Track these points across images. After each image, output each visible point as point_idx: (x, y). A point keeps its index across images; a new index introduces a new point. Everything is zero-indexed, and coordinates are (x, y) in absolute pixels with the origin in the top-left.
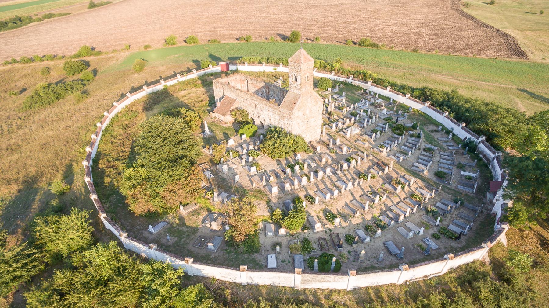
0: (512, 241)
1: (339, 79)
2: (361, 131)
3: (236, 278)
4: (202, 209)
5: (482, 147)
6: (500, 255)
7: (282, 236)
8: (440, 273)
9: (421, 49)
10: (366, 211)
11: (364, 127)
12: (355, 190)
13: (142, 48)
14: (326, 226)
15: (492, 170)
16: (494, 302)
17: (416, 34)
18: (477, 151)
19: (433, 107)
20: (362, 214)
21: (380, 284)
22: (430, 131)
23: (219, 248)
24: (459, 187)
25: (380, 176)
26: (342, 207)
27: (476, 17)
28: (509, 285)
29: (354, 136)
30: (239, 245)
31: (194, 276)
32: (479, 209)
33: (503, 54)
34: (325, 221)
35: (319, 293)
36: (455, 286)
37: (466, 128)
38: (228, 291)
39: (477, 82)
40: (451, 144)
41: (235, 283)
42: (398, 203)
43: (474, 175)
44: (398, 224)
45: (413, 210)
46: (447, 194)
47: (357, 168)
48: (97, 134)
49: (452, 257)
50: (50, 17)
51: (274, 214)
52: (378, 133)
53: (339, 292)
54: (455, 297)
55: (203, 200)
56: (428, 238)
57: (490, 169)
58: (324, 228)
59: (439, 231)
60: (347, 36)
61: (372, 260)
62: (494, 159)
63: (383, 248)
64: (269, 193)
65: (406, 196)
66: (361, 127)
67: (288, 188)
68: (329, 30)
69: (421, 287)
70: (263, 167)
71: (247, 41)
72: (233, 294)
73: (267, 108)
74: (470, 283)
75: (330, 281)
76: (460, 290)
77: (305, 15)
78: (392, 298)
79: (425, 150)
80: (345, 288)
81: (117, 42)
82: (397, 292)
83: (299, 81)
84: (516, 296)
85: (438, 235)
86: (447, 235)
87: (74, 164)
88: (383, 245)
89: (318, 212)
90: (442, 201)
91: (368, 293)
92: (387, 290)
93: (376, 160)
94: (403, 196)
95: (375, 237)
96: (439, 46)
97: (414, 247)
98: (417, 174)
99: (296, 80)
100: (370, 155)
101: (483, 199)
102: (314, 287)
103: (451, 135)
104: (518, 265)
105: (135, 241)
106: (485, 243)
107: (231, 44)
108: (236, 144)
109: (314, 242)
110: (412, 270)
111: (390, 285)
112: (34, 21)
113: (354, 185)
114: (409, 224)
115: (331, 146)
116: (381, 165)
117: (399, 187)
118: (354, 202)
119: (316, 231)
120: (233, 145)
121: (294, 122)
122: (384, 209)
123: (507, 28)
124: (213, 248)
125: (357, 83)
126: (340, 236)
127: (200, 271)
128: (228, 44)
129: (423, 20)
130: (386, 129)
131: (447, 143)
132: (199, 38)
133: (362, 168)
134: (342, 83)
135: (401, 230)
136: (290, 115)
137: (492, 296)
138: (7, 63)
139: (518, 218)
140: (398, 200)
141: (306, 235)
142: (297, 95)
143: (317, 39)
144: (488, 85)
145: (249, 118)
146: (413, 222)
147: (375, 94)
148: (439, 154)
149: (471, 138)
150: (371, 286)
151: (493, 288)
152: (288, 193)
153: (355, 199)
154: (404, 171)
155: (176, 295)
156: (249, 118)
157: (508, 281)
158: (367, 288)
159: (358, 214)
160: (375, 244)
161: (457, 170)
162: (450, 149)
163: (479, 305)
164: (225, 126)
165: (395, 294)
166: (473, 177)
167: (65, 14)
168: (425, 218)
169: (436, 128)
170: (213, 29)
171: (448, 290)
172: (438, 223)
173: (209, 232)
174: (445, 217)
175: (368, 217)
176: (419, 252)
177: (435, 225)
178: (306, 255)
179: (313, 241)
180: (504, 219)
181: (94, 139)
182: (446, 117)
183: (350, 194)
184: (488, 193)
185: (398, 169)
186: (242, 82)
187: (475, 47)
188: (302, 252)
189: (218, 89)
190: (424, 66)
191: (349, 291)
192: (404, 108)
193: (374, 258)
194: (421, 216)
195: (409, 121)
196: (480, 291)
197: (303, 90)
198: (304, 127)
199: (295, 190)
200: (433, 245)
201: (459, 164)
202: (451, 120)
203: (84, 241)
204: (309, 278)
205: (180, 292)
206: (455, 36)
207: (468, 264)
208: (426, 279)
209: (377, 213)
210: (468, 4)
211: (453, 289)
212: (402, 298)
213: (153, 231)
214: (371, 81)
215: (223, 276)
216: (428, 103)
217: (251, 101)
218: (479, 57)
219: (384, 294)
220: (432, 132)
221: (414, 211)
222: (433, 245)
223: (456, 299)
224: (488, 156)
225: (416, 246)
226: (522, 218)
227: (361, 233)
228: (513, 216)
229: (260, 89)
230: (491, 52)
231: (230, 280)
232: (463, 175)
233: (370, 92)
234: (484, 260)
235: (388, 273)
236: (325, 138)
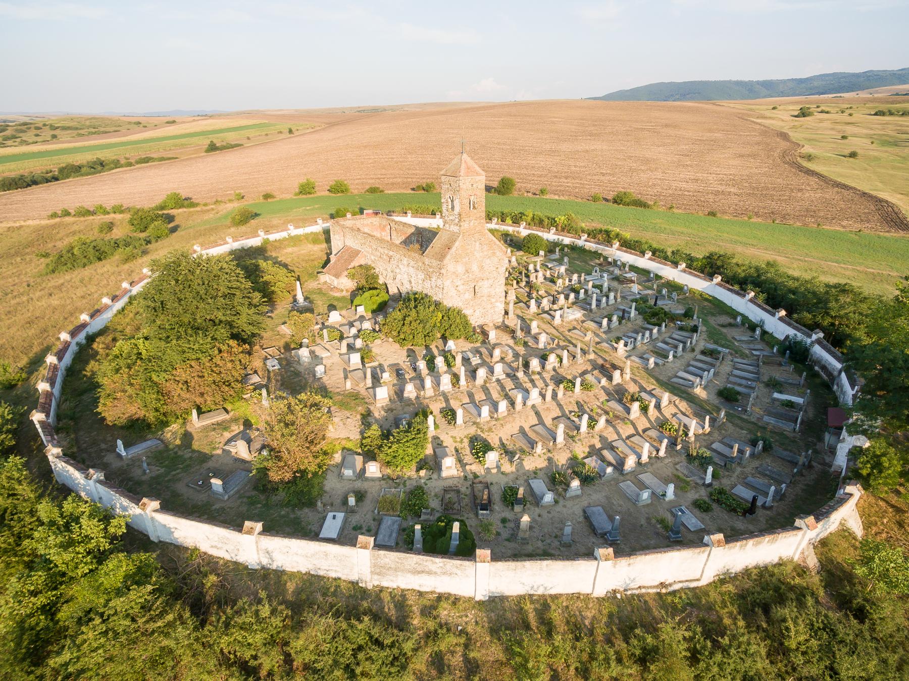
0: (874, 529)
1: (562, 240)
2: (584, 315)
6: (845, 556)
7: (373, 480)
8: (698, 580)
9: (724, 213)
10: (559, 446)
11: (591, 310)
12: (545, 407)
13: (261, 198)
14: (468, 467)
15: (838, 394)
16: (820, 659)
17: (717, 193)
19: (727, 285)
20: (549, 451)
21: (553, 592)
22: (719, 325)
23: (238, 491)
24: (766, 418)
25: (603, 388)
26: (512, 436)
27: (825, 174)
28: (862, 622)
30: (277, 489)
31: (160, 542)
32: (802, 460)
33: (874, 226)
34: (468, 458)
35: (411, 600)
36: (731, 614)
37: (787, 319)
38: (213, 578)
39: (822, 263)
40: (759, 347)
41: (236, 563)
42: (629, 437)
43: (800, 400)
44: (623, 475)
45: (658, 451)
46: (738, 429)
47: (561, 371)
48: (114, 298)
49: (719, 541)
50: (147, 162)
51: (366, 435)
52: (615, 318)
53: (456, 601)
54: (722, 637)
56: (683, 508)
57: (834, 392)
58: (464, 470)
59: (711, 494)
60: (595, 190)
61: (548, 541)
63: (581, 519)
64: (372, 400)
65: (649, 426)
66: (584, 309)
67: (410, 392)
68: (568, 183)
69: (648, 610)
70: (379, 358)
71: (427, 191)
72: (223, 586)
73: (405, 261)
74: (766, 610)
75: (436, 573)
76: (741, 623)
77: (531, 162)
78: (576, 626)
79: (703, 353)
82: (589, 614)
84: (877, 649)
85: (705, 502)
88: (582, 514)
89: (459, 440)
90: (725, 440)
91: (522, 609)
92: (567, 607)
93: (600, 361)
94: (643, 424)
95: (568, 495)
96: (756, 210)
97: (649, 523)
98: (681, 391)
99: (453, 208)
100: (589, 350)
101: (815, 445)
102: (403, 586)
103: (758, 332)
104: (884, 576)
105: (71, 465)
106: (801, 518)
107: (400, 194)
108: (345, 321)
109: (436, 495)
110: (623, 562)
111: (576, 597)
112: (122, 166)
113: (543, 396)
114: (646, 478)
115: (519, 334)
116: (606, 370)
117: (635, 406)
119: (445, 474)
120: (337, 323)
121: (447, 283)
122: (598, 446)
123: (880, 191)
124: (220, 490)
125: (591, 246)
126: (494, 489)
127: (169, 531)
128: (395, 195)
129: (731, 175)
130: (632, 315)
131: (752, 346)
133: (569, 372)
134: (567, 246)
135: (628, 486)
137: (814, 643)
138: (54, 215)
139: (880, 472)
140: (632, 431)
141: (423, 481)
142: (453, 234)
143: (542, 192)
144: (844, 269)
145: (381, 283)
146: (655, 474)
147: (624, 265)
148: (732, 361)
149: (796, 335)
150: (531, 596)
151: (821, 626)
152: (409, 402)
153: (541, 422)
154: (655, 382)
156: (381, 283)
157: (861, 614)
158: (521, 598)
159: (539, 449)
160: (565, 510)
161: (766, 390)
162: (756, 355)
163: (786, 666)
164: (337, 295)
165: (583, 618)
166: (798, 404)
167: (169, 159)
168: (683, 468)
169: (732, 321)
170: (379, 176)
171: (713, 623)
172: (709, 479)
173: (231, 462)
174: (728, 470)
175: (562, 459)
176: (657, 534)
177: (704, 484)
178: (409, 518)
179: (433, 494)
180: (855, 476)
182: (751, 301)
183: (533, 413)
184: (826, 434)
185: (642, 378)
186: (383, 228)
187: (822, 214)
188: (401, 512)
189: (337, 237)
190: (725, 235)
192: (674, 287)
193: (556, 537)
194: (676, 464)
195: (680, 307)
196: (787, 629)
197: (465, 225)
198: (469, 296)
199: (424, 398)
200: (692, 521)
201: (771, 379)
202: (759, 306)
204: (387, 560)
205: (97, 568)
206: (786, 197)
207: (766, 567)
208: (664, 591)
209: (580, 451)
210: (810, 156)
211: (727, 621)
212: (600, 631)
213: (124, 453)
214: (617, 244)
215: (214, 544)
218: (828, 227)
219: (556, 616)
220: (723, 326)
221: (662, 453)
222: (692, 521)
223: (725, 641)
224: (829, 367)
225: (654, 521)
226: (890, 472)
227: (539, 485)
228: (869, 466)
229: (408, 238)
230: (850, 223)
231: (227, 557)
232: (778, 400)
233: (615, 261)
234: (804, 562)
235: (568, 564)
236: (513, 322)
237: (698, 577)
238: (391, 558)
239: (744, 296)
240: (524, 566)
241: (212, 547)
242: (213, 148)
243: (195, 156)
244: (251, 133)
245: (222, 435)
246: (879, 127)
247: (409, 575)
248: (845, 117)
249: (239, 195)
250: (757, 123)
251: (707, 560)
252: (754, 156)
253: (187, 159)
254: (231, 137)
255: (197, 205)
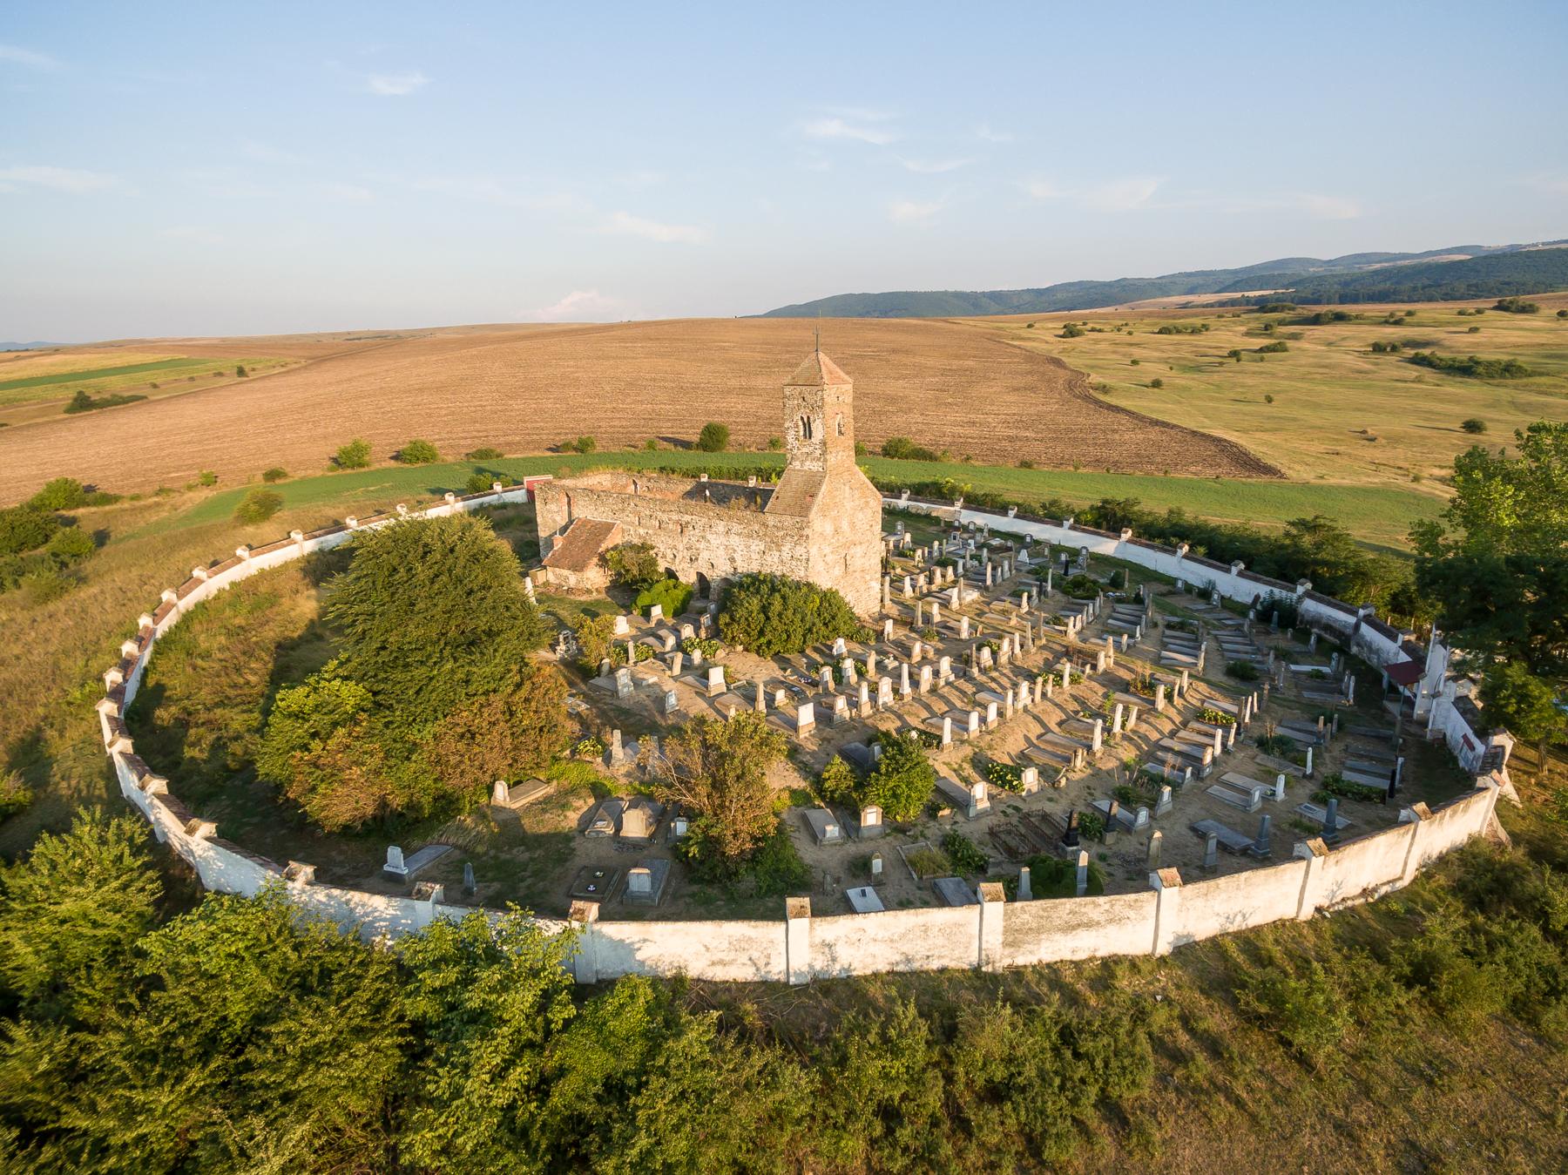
3: (769, 956)
4: (573, 791)
5: (1311, 607)
8: (1400, 878)
15: (1365, 655)
17: (1011, 439)
18: (1301, 622)
27: (1133, 409)
29: (970, 605)
41: (764, 983)
44: (1202, 780)
53: (1133, 964)
55: (571, 765)
62: (1357, 627)
66: (979, 588)
71: (582, 451)
73: (721, 527)
75: (1098, 923)
80: (1147, 949)
81: (169, 473)
83: (818, 433)
86: (1353, 793)
87: (50, 733)
88: (1191, 834)
99: (808, 433)
118: (1049, 737)
121: (814, 550)
127: (627, 949)
132: (437, 444)
136: (802, 528)
142: (812, 475)
155: (567, 1023)
181: (146, 628)
187: (1159, 459)
189: (553, 507)
191: (1162, 959)
197: (831, 458)
203: (124, 922)
216: (1128, 534)
217: (665, 517)
224: (1336, 625)
228: (1514, 700)
237: (1398, 873)
238: (1030, 910)
239: (1174, 553)
240: (1218, 885)
241: (713, 964)
242: (82, 404)
243: (46, 419)
244: (159, 377)
245: (565, 816)
246: (1171, 348)
247: (1058, 937)
248: (1122, 336)
249: (206, 476)
250: (1015, 346)
251: (1411, 844)
252: (1033, 389)
253: (29, 426)
254: (117, 385)
255: (114, 499)
